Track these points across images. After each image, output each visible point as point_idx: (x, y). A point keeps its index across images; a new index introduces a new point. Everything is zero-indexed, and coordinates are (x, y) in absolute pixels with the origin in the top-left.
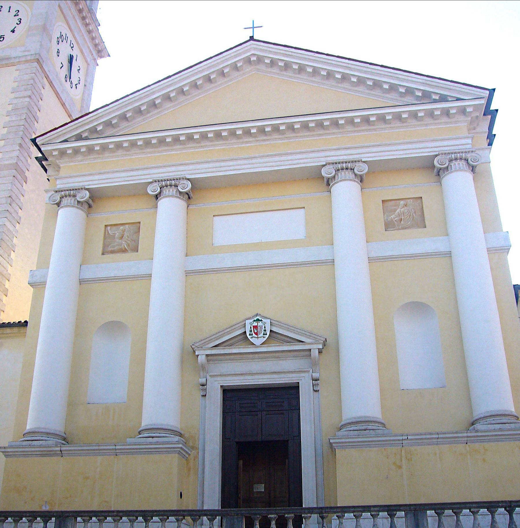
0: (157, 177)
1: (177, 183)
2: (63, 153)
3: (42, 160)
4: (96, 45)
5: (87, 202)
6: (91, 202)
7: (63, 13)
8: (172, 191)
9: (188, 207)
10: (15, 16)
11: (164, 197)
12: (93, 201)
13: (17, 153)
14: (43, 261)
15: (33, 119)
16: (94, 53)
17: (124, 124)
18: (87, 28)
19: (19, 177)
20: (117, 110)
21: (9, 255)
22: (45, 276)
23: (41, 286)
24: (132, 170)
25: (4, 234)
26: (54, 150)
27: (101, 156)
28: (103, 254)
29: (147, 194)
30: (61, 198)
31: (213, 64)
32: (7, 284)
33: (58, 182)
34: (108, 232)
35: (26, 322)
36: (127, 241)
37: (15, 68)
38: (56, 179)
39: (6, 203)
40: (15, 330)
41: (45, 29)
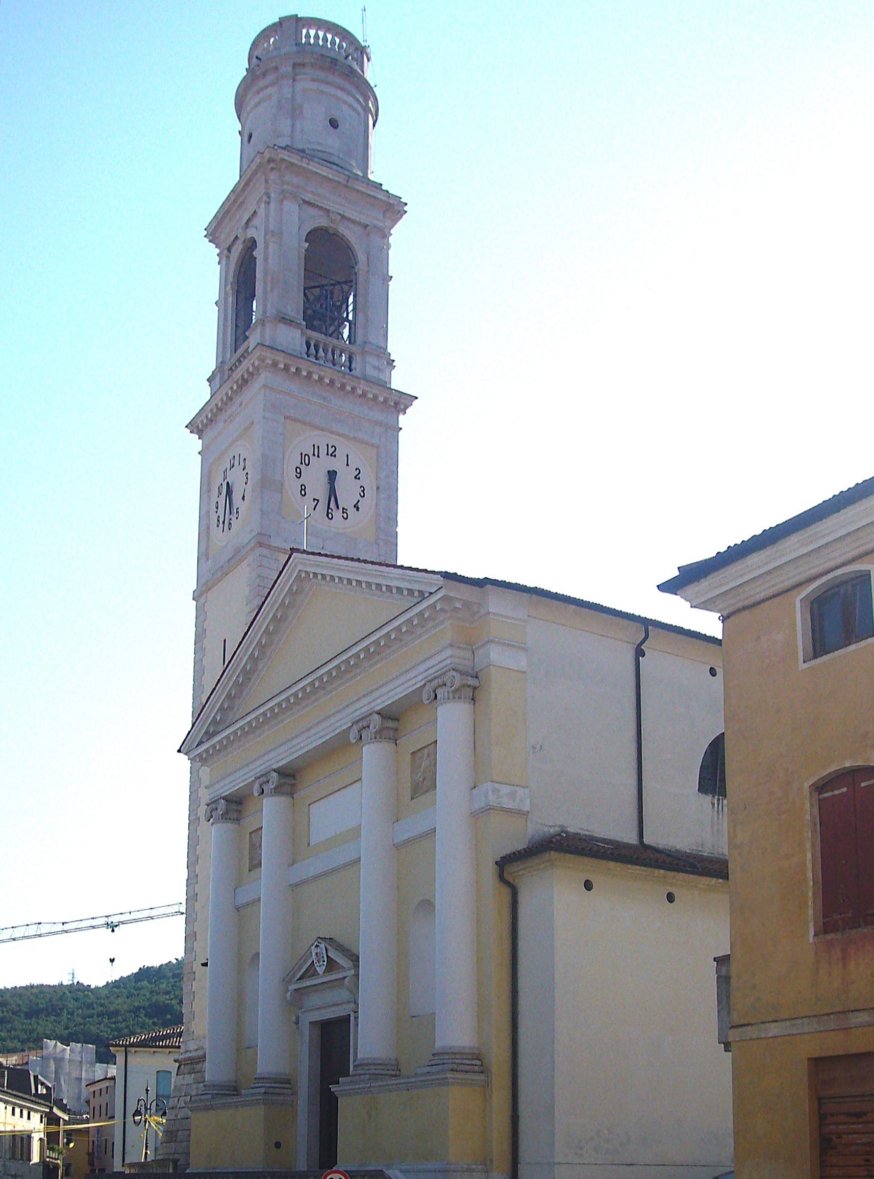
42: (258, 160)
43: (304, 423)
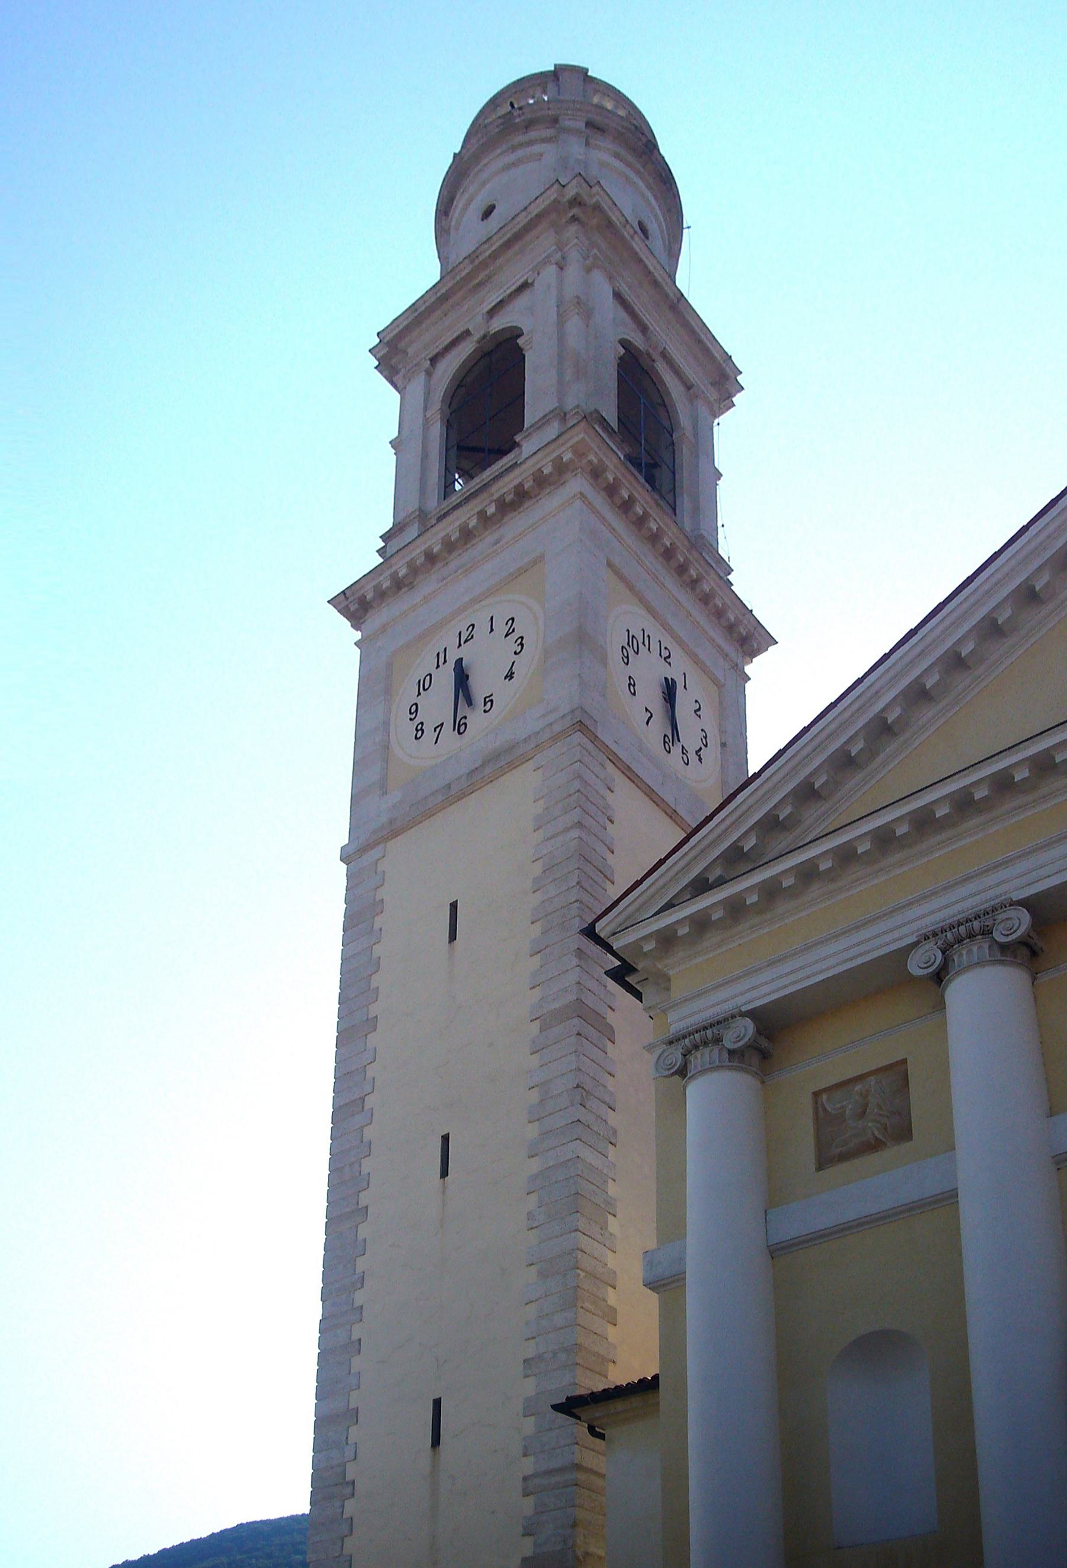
0: (930, 922)
1: (989, 923)
2: (667, 940)
3: (622, 974)
4: (731, 628)
5: (753, 1047)
6: (764, 1043)
7: (622, 578)
8: (979, 949)
9: (1034, 979)
10: (507, 635)
11: (958, 973)
12: (768, 1039)
13: (573, 977)
14: (671, 1224)
15: (600, 878)
16: (730, 649)
17: (812, 813)
18: (698, 591)
19: (593, 1033)
20: (785, 779)
21: (604, 1227)
22: (681, 1260)
23: (674, 1285)
24: (857, 928)
25: (579, 1179)
26: (644, 938)
27: (768, 916)
28: (820, 1168)
29: (912, 979)
30: (686, 1054)
31: (1033, 545)
32: (612, 1297)
33: (672, 1016)
34: (825, 1109)
35: (656, 1377)
36: (881, 1117)
37: (530, 765)
38: (664, 1012)
39: (572, 1105)
40: (635, 1401)
41: (583, 640)
42: (552, 194)
43: (631, 588)
